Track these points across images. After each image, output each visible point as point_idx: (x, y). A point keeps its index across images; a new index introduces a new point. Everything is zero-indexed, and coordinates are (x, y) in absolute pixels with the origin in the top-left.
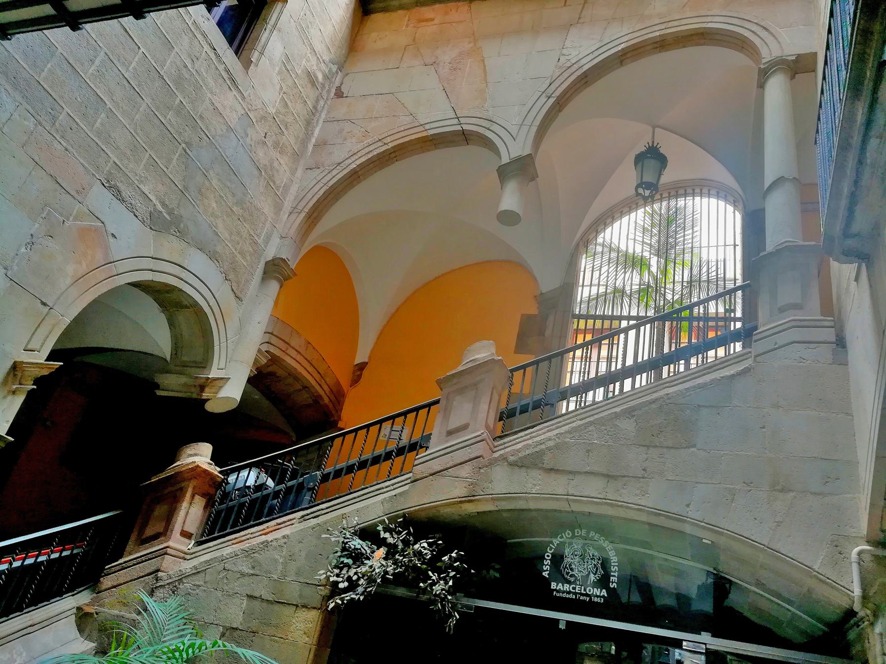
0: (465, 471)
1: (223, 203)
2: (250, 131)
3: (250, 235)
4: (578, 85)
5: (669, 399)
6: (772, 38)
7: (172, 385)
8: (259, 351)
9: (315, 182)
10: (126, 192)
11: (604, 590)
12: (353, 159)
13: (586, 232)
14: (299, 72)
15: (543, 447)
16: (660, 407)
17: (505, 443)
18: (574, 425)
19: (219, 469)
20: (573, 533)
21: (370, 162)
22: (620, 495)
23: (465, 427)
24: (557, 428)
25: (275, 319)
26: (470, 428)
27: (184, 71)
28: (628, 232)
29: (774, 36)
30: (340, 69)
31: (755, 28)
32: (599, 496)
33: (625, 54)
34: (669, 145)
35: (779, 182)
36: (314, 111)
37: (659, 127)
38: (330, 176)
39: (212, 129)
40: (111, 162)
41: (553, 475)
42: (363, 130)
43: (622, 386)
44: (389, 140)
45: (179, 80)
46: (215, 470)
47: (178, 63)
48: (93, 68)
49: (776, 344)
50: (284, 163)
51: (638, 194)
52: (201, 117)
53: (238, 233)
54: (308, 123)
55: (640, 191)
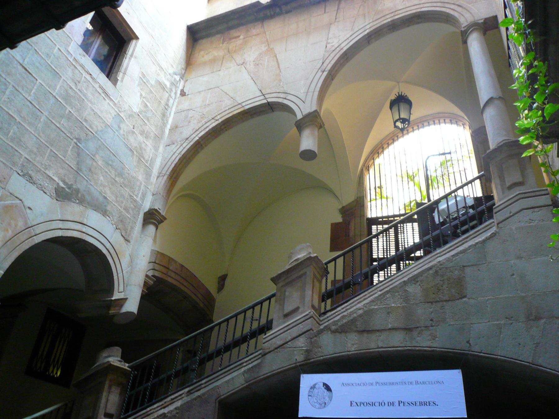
2: (122, 126)
3: (131, 196)
6: (465, 11)
8: (147, 276)
10: (37, 177)
12: (196, 134)
13: (366, 161)
14: (153, 83)
15: (355, 315)
16: (436, 272)
17: (328, 317)
18: (376, 295)
19: (127, 365)
22: (417, 342)
23: (295, 310)
24: (365, 299)
26: (300, 310)
29: (467, 10)
30: (182, 77)
31: (452, 7)
33: (370, 36)
34: (411, 93)
35: (490, 101)
38: (182, 148)
39: (94, 127)
40: (23, 157)
41: (365, 335)
45: (67, 98)
48: (5, 97)
49: (510, 213)
50: (149, 145)
52: (86, 120)
53: (123, 196)
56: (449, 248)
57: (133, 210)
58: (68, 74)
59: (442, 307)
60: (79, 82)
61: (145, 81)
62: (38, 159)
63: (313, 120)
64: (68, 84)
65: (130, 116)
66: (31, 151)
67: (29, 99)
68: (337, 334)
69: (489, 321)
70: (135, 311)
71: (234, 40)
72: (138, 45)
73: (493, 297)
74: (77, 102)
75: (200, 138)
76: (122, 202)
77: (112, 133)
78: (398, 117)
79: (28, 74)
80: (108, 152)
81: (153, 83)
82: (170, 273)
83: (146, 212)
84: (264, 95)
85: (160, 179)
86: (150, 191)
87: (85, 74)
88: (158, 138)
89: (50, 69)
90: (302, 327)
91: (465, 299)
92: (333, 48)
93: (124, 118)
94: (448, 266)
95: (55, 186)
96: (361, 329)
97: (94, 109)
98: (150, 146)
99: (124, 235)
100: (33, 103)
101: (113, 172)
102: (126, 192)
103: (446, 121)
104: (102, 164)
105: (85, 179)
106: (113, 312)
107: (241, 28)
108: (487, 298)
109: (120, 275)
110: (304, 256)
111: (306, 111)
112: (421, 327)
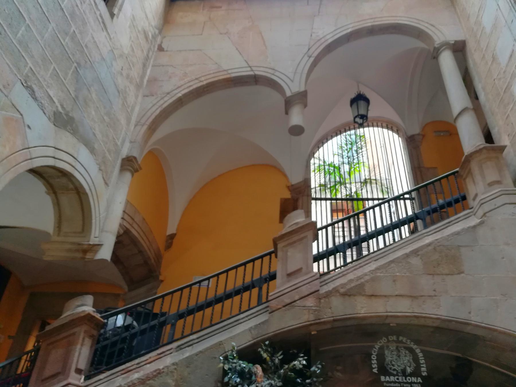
0: (310, 302)
2: (114, 63)
3: (114, 139)
7: (55, 253)
9: (151, 105)
11: (419, 378)
15: (362, 280)
16: (435, 249)
17: (325, 281)
20: (388, 339)
21: (191, 93)
25: (128, 202)
27: (76, 9)
28: (331, 151)
30: (160, 32)
31: (426, 25)
36: (147, 58)
45: (73, 14)
46: (98, 316)
49: (495, 205)
51: (355, 122)
54: (144, 66)
78: (356, 114)
81: (140, 29)
84: (250, 67)
85: (138, 128)
90: (309, 287)
91: (462, 275)
99: (104, 176)
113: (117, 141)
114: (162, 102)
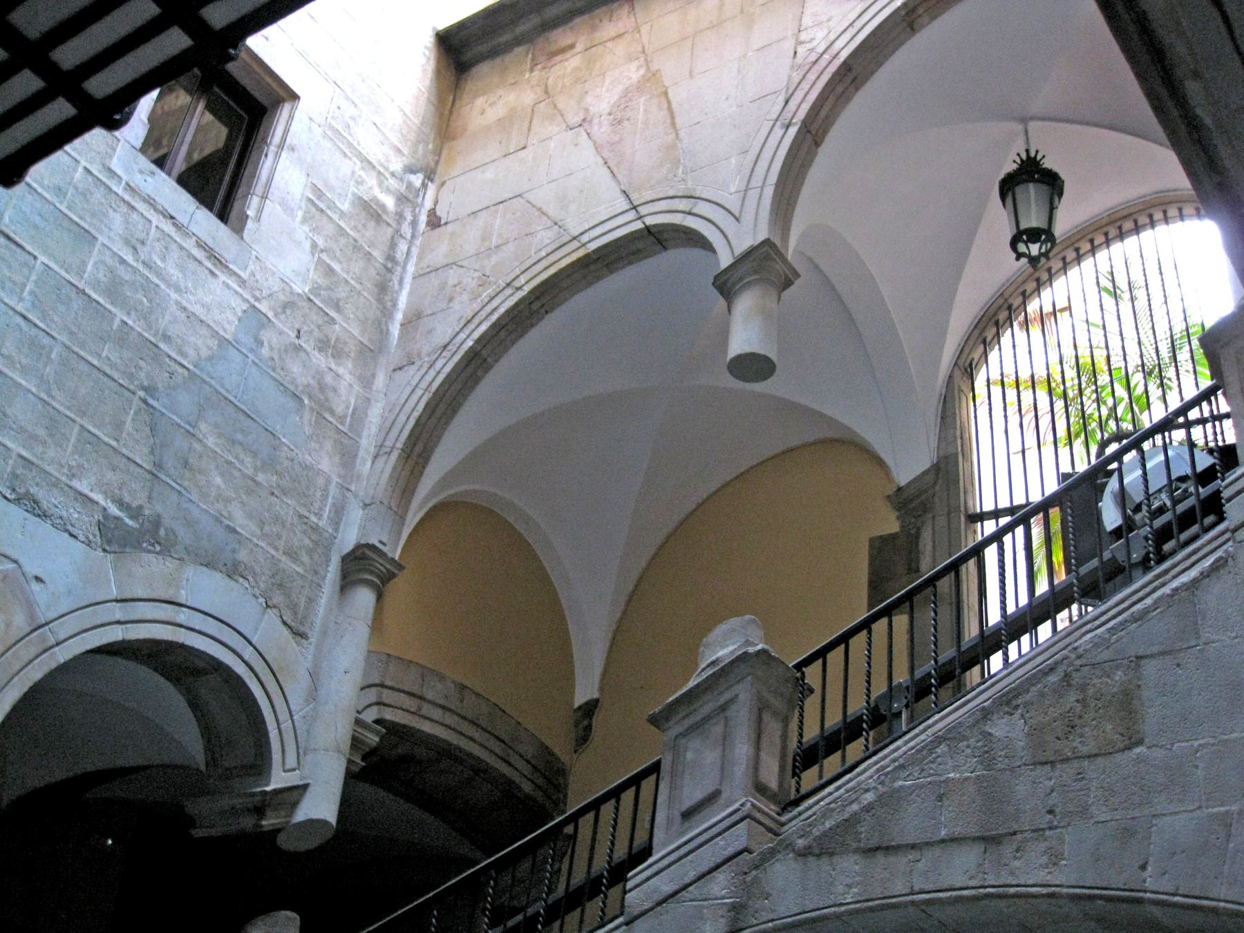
0: (720, 885)
1: (237, 474)
2: (266, 335)
3: (301, 516)
4: (839, 89)
5: (1079, 657)
8: (358, 722)
10: (50, 499)
12: (467, 331)
21: (498, 327)
22: (1012, 873)
23: (713, 798)
25: (379, 656)
26: (724, 795)
30: (430, 176)
32: (972, 883)
37: (1032, 119)
38: (432, 373)
39: (191, 352)
40: (14, 456)
41: (880, 858)
42: (477, 274)
43: (1006, 655)
44: (522, 280)
45: (114, 289)
47: (109, 261)
50: (346, 371)
52: (166, 338)
53: (277, 519)
55: (1022, 248)
56: (1117, 604)
57: (310, 552)
58: (112, 232)
59: (1080, 776)
60: (143, 243)
61: (322, 205)
62: (51, 453)
63: (764, 265)
64: (115, 254)
65: (285, 306)
66: (34, 437)
67: (19, 308)
68: (811, 859)
69: (1200, 807)
70: (332, 818)
71: (559, 58)
72: (298, 114)
73: (1212, 741)
74: (139, 296)
75: (478, 341)
76: (279, 537)
77: (238, 358)
79: (13, 246)
80: (231, 409)
81: (345, 206)
82: (427, 709)
83: (349, 555)
86: (356, 496)
87: (156, 219)
88: (370, 354)
89: (66, 223)
91: (1138, 750)
92: (813, 58)
93: (270, 315)
94: (1099, 659)
95: (98, 516)
96: (873, 843)
97: (185, 304)
98: (348, 377)
99: (289, 622)
100: (30, 316)
101: (248, 460)
102: (288, 507)
103: (1185, 212)
104: (217, 444)
105: (173, 488)
106: (272, 821)
107: (577, 20)
108: (1196, 744)
109: (286, 725)
110: (732, 652)
111: (742, 246)
112: (1022, 832)
113: (314, 519)
114: (428, 378)
